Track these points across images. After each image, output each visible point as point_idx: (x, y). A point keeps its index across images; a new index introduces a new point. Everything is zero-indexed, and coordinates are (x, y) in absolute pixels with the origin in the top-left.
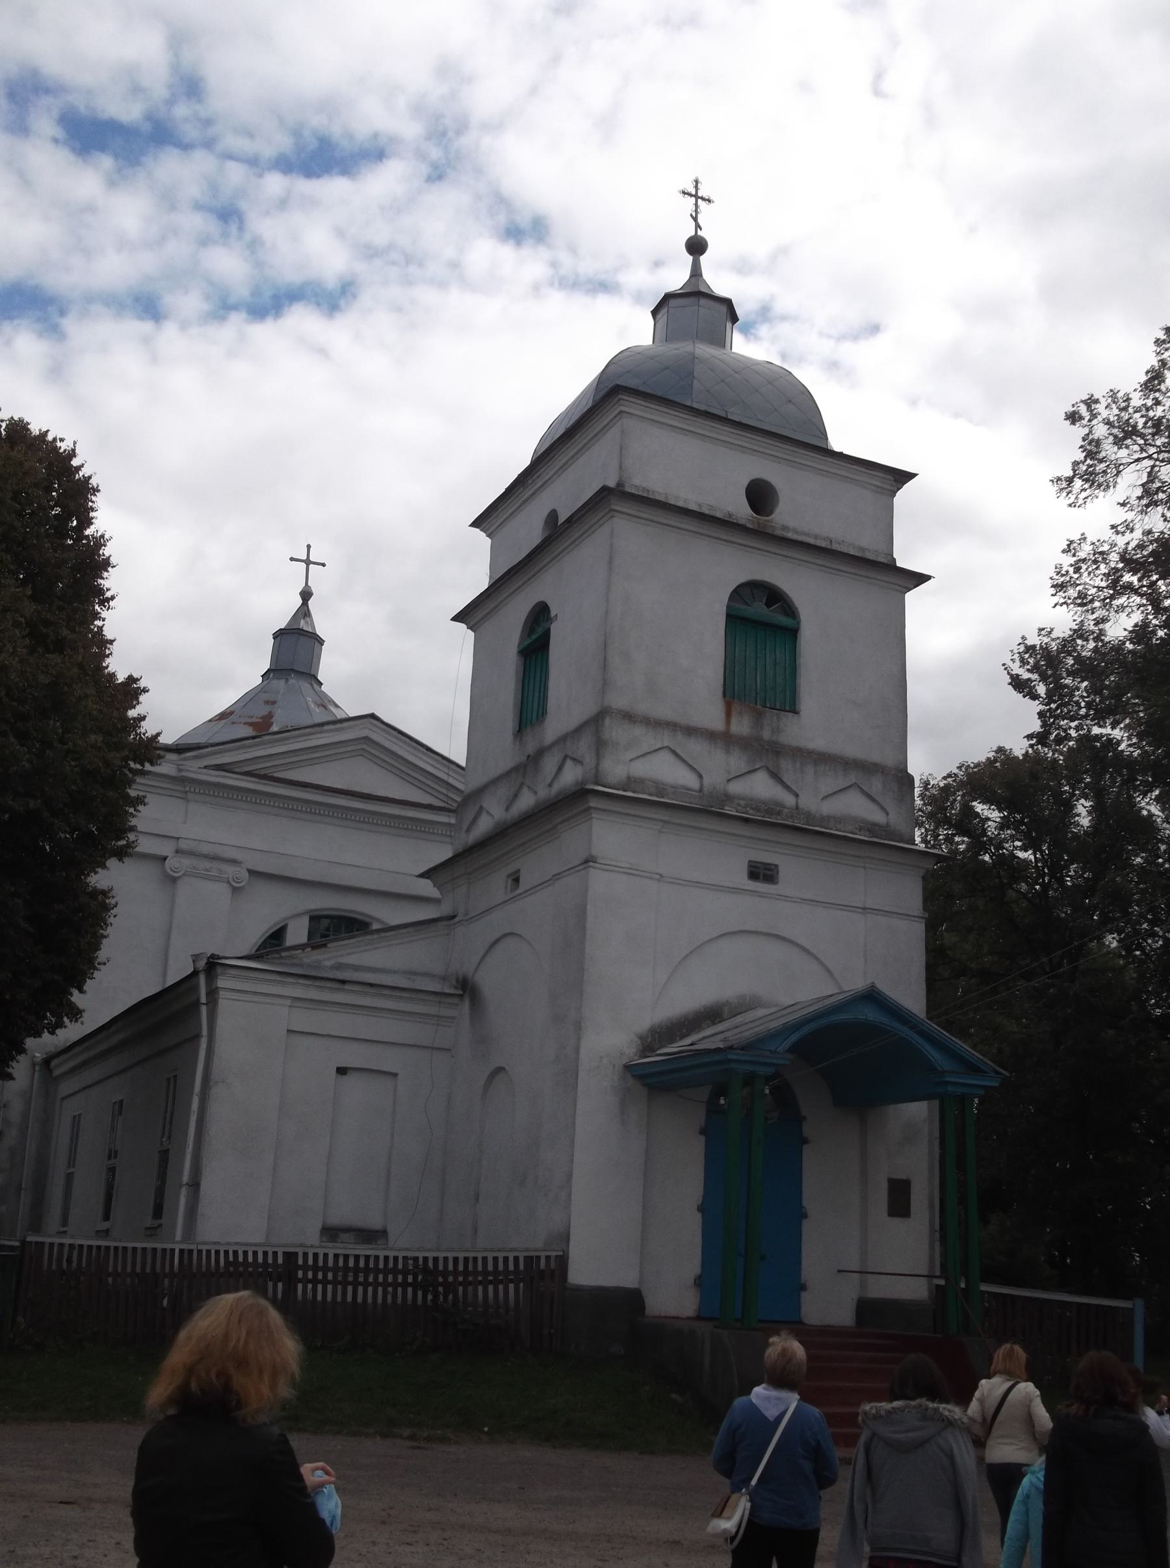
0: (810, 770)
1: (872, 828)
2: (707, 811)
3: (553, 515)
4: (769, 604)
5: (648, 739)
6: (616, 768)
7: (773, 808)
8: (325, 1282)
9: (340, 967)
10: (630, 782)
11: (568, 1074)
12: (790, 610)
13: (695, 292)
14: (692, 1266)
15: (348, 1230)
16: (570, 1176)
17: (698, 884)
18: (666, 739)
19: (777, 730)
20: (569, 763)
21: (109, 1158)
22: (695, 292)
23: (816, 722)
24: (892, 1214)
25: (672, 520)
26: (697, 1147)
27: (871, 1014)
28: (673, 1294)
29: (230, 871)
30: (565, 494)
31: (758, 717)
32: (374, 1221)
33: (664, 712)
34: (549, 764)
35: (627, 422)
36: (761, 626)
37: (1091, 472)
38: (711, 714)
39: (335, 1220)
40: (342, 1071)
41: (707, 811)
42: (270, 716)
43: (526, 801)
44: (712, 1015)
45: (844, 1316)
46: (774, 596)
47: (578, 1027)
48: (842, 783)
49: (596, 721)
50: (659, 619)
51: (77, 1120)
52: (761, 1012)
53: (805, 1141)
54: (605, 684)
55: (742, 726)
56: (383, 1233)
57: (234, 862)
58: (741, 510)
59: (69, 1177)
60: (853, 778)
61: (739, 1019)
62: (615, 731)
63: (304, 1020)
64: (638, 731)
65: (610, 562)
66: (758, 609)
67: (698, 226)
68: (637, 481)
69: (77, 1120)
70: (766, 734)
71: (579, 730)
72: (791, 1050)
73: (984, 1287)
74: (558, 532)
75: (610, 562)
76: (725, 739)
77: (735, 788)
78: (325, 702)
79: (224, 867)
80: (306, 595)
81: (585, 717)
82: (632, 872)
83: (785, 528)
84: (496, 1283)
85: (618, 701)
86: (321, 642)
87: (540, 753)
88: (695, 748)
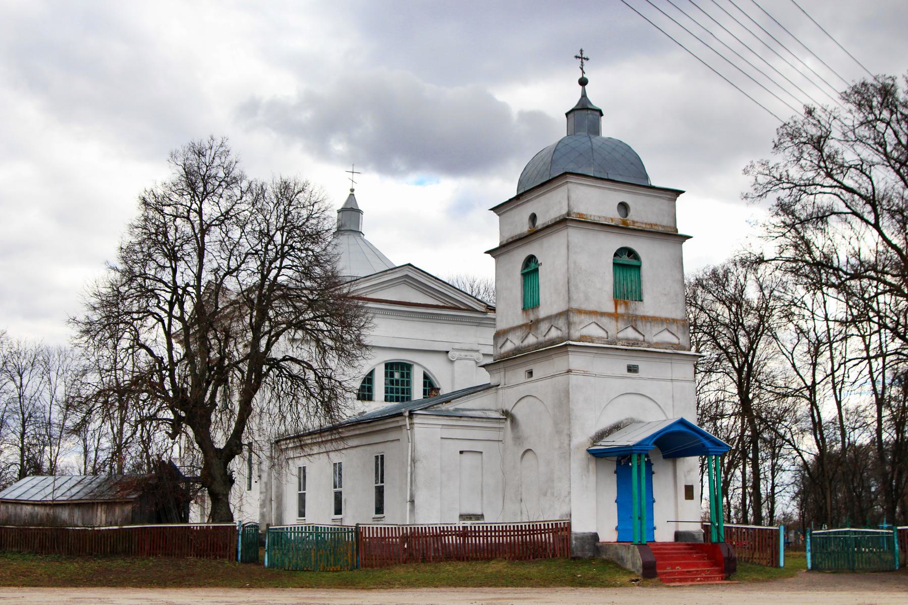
2: (610, 348)
4: (628, 256)
7: (636, 342)
9: (456, 410)
10: (582, 338)
14: (615, 523)
16: (569, 493)
17: (609, 376)
20: (553, 329)
21: (335, 487)
25: (590, 227)
26: (615, 477)
27: (682, 428)
28: (608, 535)
31: (626, 304)
32: (478, 511)
33: (592, 307)
34: (544, 327)
35: (570, 185)
36: (627, 263)
38: (609, 307)
40: (461, 452)
43: (531, 340)
44: (617, 427)
45: (670, 538)
46: (631, 253)
47: (569, 436)
49: (565, 314)
51: (303, 471)
53: (653, 473)
55: (621, 310)
62: (575, 318)
63: (448, 433)
64: (583, 317)
66: (625, 259)
67: (583, 72)
68: (575, 211)
70: (631, 312)
71: (559, 315)
74: (535, 233)
76: (615, 316)
80: (352, 190)
81: (560, 310)
82: (585, 374)
83: (634, 222)
85: (574, 305)
88: (605, 321)
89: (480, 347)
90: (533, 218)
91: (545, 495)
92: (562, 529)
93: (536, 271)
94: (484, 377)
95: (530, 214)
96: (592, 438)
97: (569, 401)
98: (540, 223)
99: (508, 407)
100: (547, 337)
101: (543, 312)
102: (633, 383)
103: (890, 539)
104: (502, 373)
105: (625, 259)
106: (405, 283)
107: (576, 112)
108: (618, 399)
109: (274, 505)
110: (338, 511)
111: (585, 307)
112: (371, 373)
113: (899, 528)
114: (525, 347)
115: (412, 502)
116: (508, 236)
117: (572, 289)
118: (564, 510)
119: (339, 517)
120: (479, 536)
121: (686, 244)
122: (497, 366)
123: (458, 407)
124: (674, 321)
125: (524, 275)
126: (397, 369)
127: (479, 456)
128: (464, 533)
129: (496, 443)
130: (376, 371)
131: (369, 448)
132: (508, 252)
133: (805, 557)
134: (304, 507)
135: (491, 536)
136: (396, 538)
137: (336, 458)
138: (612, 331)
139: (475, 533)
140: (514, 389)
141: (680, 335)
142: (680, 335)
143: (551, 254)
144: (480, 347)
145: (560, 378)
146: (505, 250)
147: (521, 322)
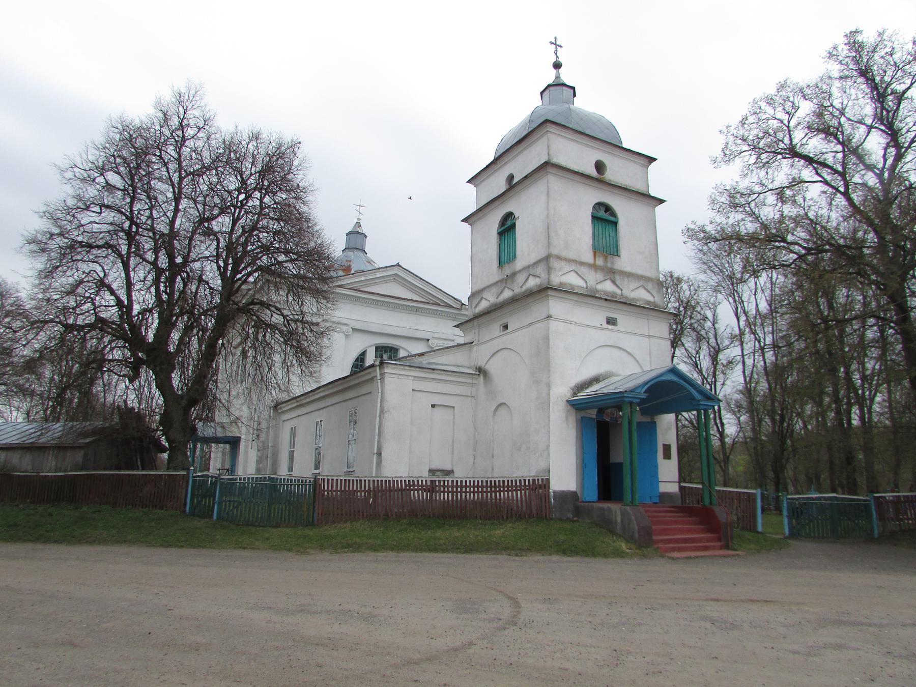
0: (626, 279)
1: (649, 303)
2: (591, 296)
3: (511, 177)
4: (606, 212)
5: (567, 267)
6: (556, 280)
7: (614, 295)
8: (448, 492)
9: (430, 363)
11: (544, 405)
12: (613, 214)
13: (558, 84)
15: (439, 471)
16: (548, 446)
17: (589, 326)
18: (573, 267)
19: (613, 263)
22: (558, 84)
23: (627, 260)
24: (664, 458)
25: (571, 176)
27: (672, 377)
29: (344, 328)
30: (520, 166)
31: (606, 258)
32: (448, 467)
33: (571, 255)
34: (520, 279)
36: (604, 218)
37: (728, 156)
38: (588, 257)
39: (434, 467)
40: (433, 406)
41: (591, 296)
42: (350, 266)
43: (507, 294)
44: (596, 380)
46: (608, 209)
47: (548, 385)
48: (638, 285)
49: (547, 258)
50: (558, 219)
51: (293, 431)
52: (615, 379)
54: (549, 244)
55: (600, 262)
56: (453, 471)
57: (346, 325)
58: (593, 172)
59: (292, 454)
60: (641, 283)
61: (606, 381)
62: (555, 264)
63: (418, 385)
64: (563, 263)
65: (548, 193)
66: (602, 214)
69: (293, 431)
70: (609, 265)
71: (536, 264)
72: (645, 392)
73: (700, 486)
74: (512, 186)
75: (548, 193)
76: (594, 267)
77: (599, 287)
78: (370, 262)
79: (342, 327)
82: (565, 321)
84: (516, 490)
85: (555, 251)
86: (366, 237)
87: (514, 274)
88: (584, 270)
89: (455, 338)
90: (511, 177)
91: (519, 450)
92: (540, 487)
93: (513, 226)
94: (460, 337)
95: (507, 175)
96: (572, 389)
97: (548, 348)
98: (515, 180)
99: (481, 363)
100: (524, 288)
101: (519, 264)
102: (608, 336)
103: (867, 507)
104: (476, 331)
105: (602, 214)
106: (395, 281)
107: (551, 88)
108: (600, 351)
109: (269, 461)
110: (317, 467)
111: (564, 254)
112: (363, 354)
113: (789, 497)
114: (500, 303)
115: (379, 454)
116: (475, 289)
117: (552, 234)
118: (542, 465)
119: (318, 471)
120: (448, 492)
121: (659, 209)
122: (471, 324)
123: (432, 361)
124: (648, 279)
125: (501, 234)
126: (386, 352)
127: (450, 411)
128: (431, 488)
129: (469, 399)
130: (368, 352)
131: (344, 404)
132: (484, 216)
133: (782, 523)
134: (292, 462)
135: (470, 492)
136: (336, 491)
137: (317, 417)
138: (591, 283)
139: (445, 488)
140: (490, 346)
141: (655, 293)
142: (655, 293)
143: (529, 210)
144: (455, 338)
145: (539, 325)
146: (481, 214)
147: (496, 279)
